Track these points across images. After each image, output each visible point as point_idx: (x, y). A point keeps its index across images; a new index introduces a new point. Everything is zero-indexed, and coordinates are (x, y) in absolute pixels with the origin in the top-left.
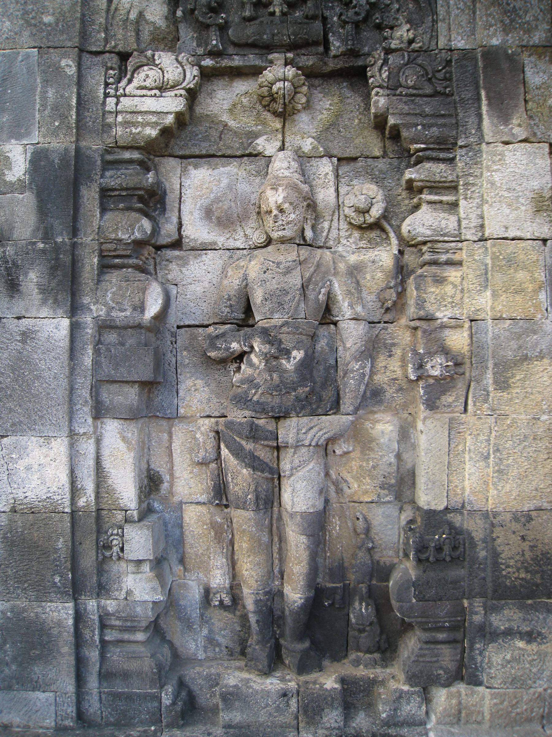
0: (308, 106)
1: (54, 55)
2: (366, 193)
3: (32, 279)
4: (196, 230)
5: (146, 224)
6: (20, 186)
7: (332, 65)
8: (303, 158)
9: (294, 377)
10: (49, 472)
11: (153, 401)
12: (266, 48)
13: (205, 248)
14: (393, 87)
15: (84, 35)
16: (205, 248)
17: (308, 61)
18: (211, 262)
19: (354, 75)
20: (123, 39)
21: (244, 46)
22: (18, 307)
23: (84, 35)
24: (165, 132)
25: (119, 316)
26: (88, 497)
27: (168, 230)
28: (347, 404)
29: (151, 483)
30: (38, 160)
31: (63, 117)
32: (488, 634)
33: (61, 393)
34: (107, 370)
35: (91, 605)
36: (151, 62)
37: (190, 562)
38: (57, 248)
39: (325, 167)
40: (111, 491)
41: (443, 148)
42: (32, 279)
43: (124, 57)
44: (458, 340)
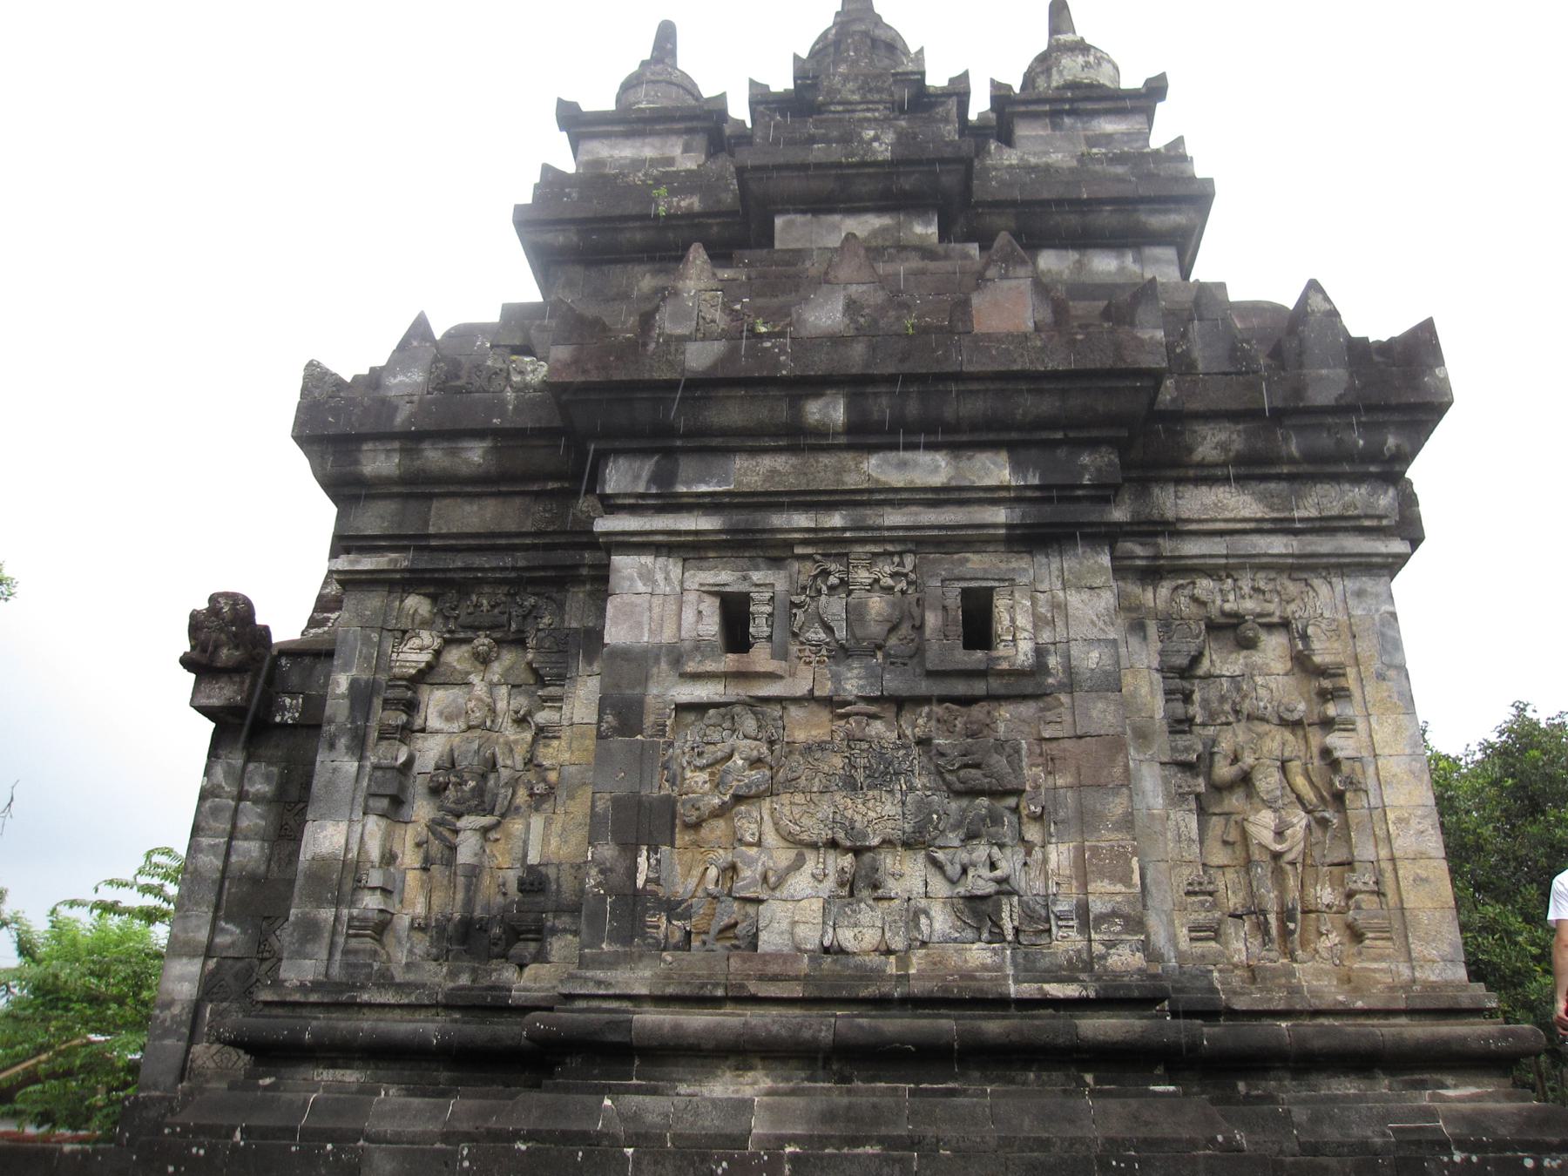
0: (497, 658)
1: (368, 631)
2: (521, 702)
3: (342, 742)
4: (434, 722)
5: (404, 717)
6: (343, 696)
7: (511, 637)
8: (492, 686)
9: (468, 795)
10: (335, 839)
11: (396, 807)
12: (476, 629)
13: (437, 732)
14: (538, 648)
15: (385, 621)
16: (437, 732)
17: (498, 635)
18: (440, 739)
19: (519, 642)
20: (405, 623)
21: (465, 628)
22: (333, 755)
23: (385, 621)
24: (420, 671)
25: (384, 762)
26: (353, 855)
27: (418, 723)
28: (497, 812)
29: (389, 858)
30: (354, 684)
31: (369, 663)
32: (554, 931)
33: (349, 799)
34: (374, 789)
35: (345, 912)
36: (418, 636)
37: (406, 903)
38: (357, 728)
39: (504, 690)
40: (367, 852)
41: (561, 679)
42: (342, 742)
43: (404, 632)
44: (552, 776)
